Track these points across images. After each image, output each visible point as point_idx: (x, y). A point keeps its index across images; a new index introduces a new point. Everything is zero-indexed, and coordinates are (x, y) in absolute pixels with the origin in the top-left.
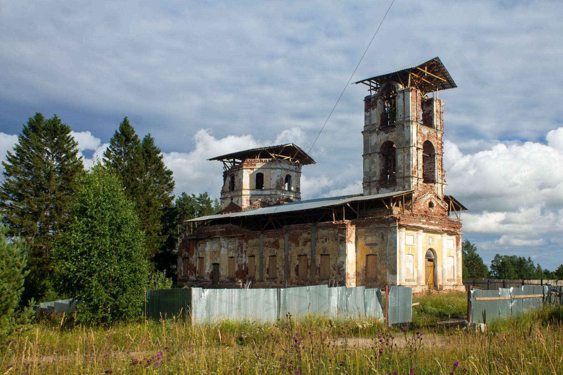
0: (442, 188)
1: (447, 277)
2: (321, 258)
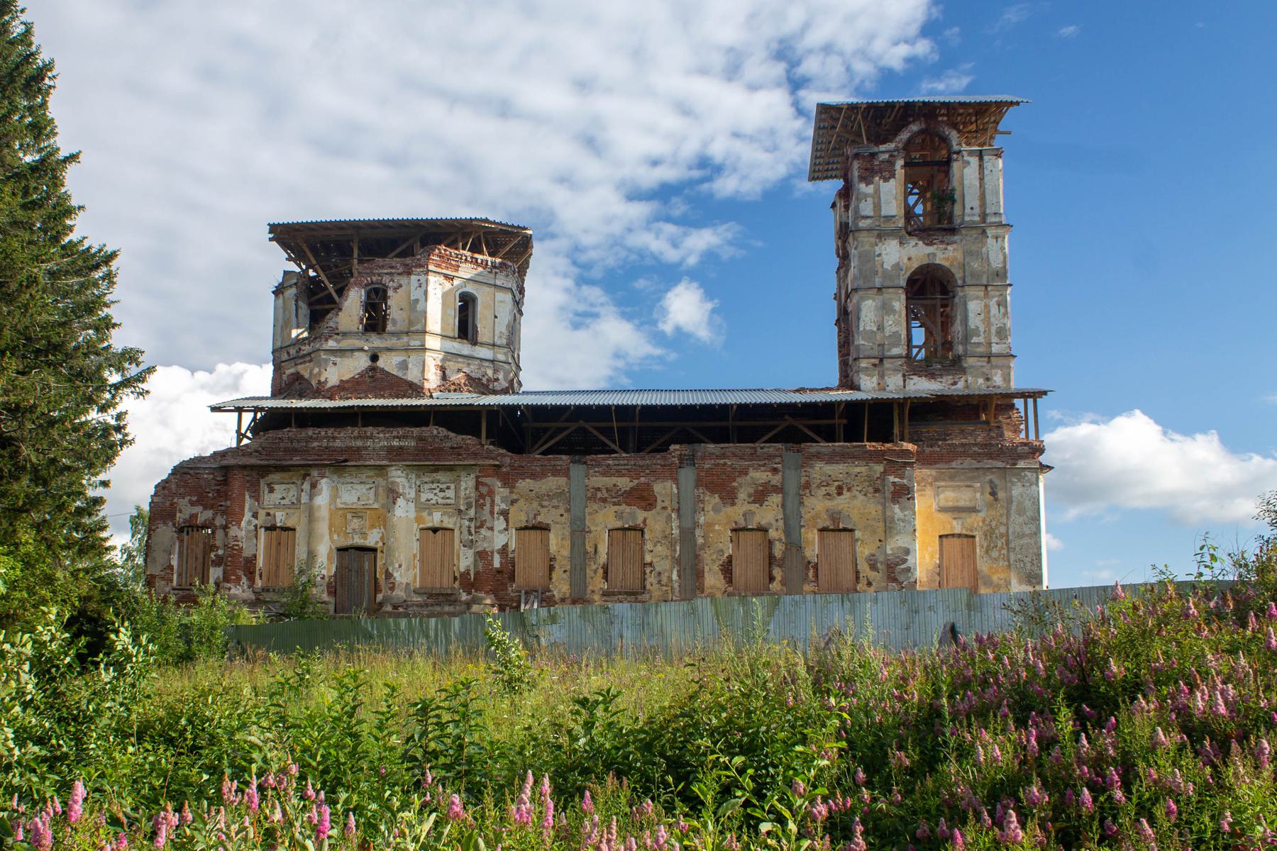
2: (821, 540)
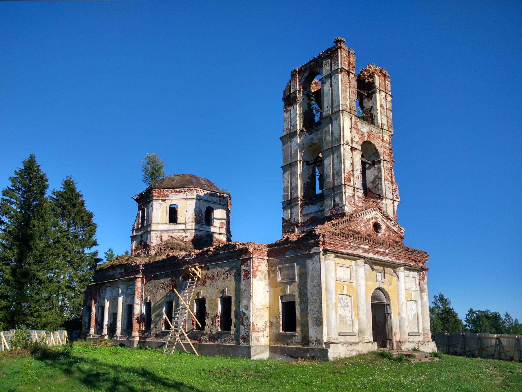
0: (394, 206)
1: (407, 330)
